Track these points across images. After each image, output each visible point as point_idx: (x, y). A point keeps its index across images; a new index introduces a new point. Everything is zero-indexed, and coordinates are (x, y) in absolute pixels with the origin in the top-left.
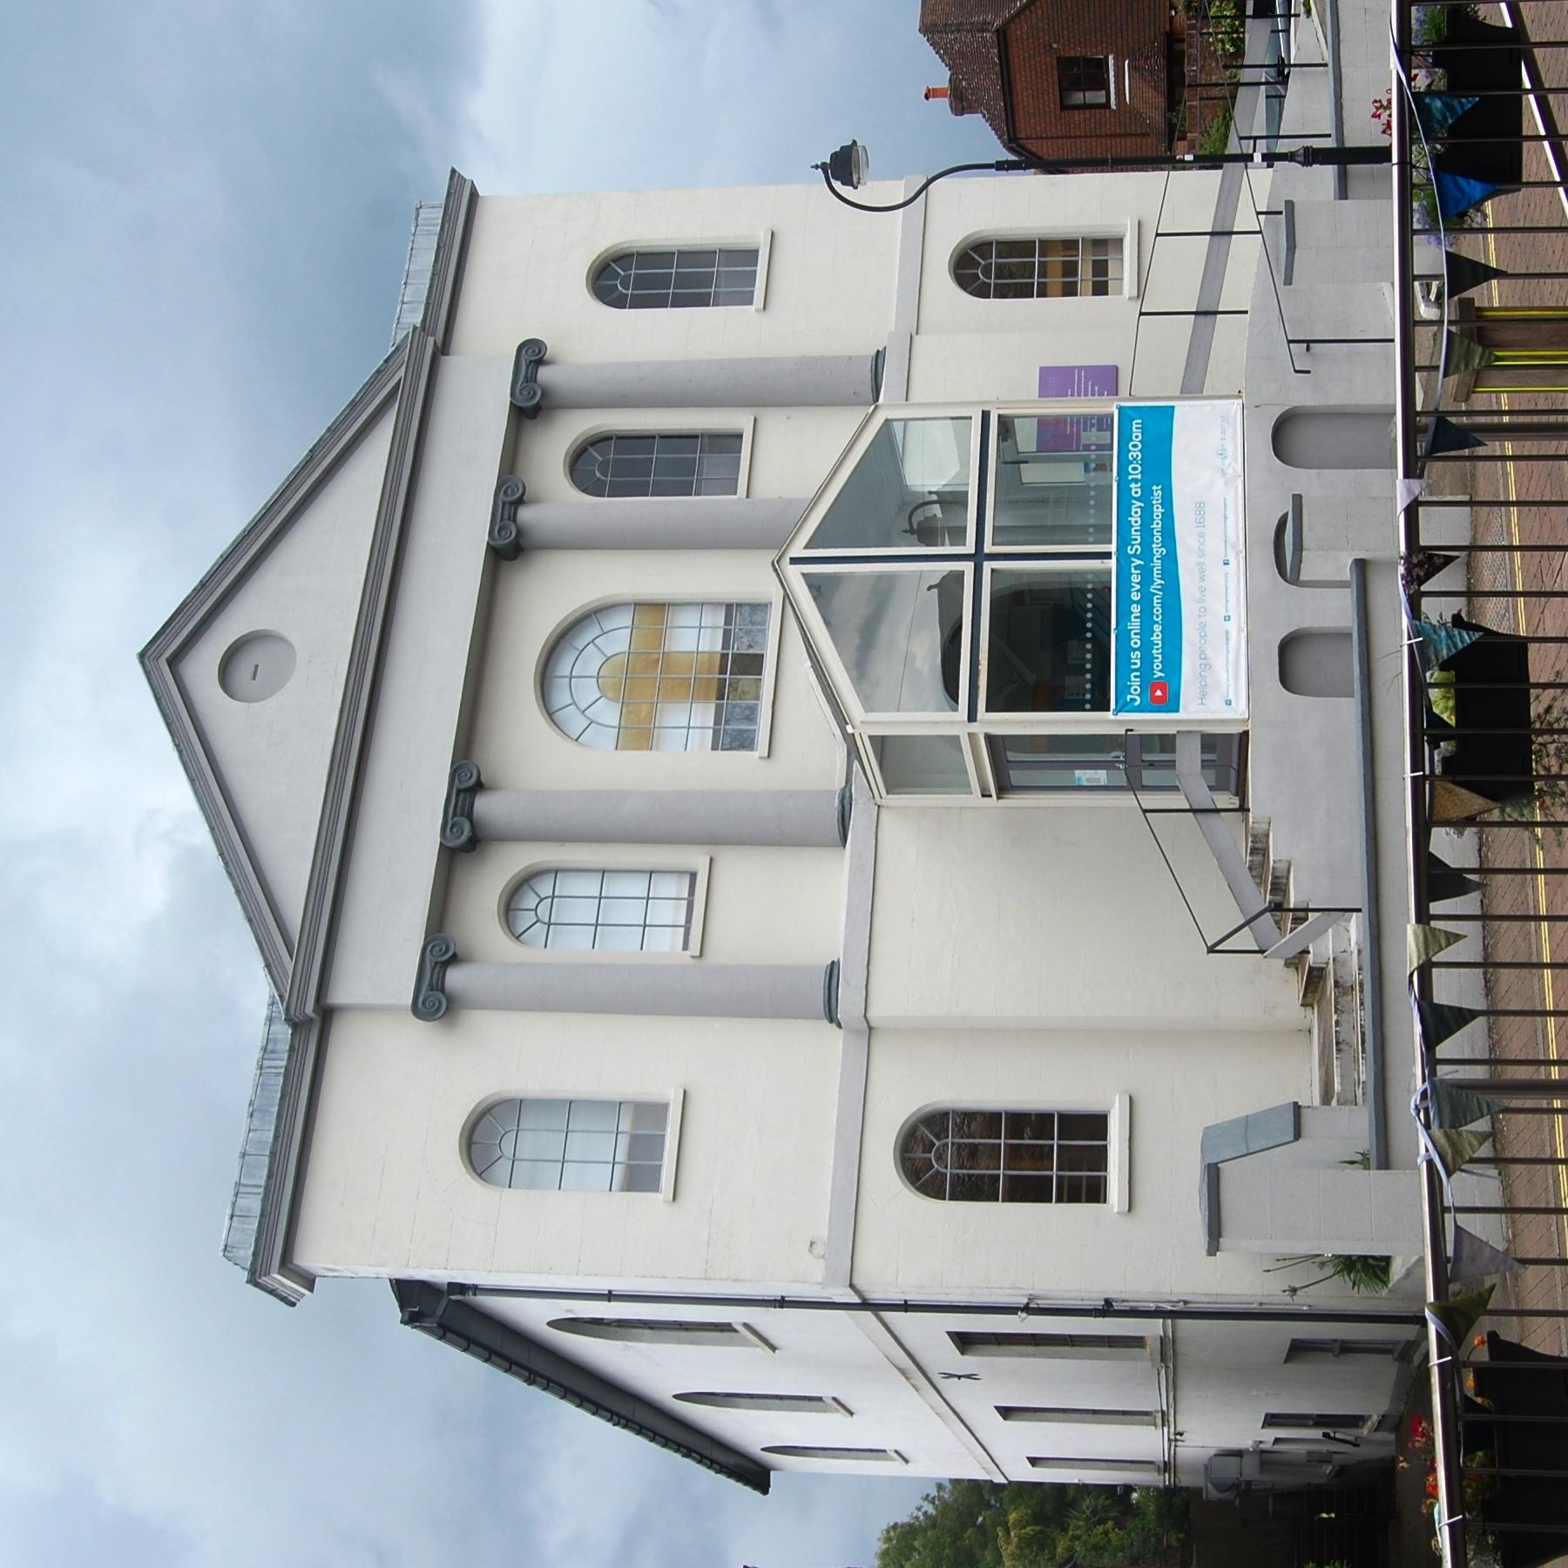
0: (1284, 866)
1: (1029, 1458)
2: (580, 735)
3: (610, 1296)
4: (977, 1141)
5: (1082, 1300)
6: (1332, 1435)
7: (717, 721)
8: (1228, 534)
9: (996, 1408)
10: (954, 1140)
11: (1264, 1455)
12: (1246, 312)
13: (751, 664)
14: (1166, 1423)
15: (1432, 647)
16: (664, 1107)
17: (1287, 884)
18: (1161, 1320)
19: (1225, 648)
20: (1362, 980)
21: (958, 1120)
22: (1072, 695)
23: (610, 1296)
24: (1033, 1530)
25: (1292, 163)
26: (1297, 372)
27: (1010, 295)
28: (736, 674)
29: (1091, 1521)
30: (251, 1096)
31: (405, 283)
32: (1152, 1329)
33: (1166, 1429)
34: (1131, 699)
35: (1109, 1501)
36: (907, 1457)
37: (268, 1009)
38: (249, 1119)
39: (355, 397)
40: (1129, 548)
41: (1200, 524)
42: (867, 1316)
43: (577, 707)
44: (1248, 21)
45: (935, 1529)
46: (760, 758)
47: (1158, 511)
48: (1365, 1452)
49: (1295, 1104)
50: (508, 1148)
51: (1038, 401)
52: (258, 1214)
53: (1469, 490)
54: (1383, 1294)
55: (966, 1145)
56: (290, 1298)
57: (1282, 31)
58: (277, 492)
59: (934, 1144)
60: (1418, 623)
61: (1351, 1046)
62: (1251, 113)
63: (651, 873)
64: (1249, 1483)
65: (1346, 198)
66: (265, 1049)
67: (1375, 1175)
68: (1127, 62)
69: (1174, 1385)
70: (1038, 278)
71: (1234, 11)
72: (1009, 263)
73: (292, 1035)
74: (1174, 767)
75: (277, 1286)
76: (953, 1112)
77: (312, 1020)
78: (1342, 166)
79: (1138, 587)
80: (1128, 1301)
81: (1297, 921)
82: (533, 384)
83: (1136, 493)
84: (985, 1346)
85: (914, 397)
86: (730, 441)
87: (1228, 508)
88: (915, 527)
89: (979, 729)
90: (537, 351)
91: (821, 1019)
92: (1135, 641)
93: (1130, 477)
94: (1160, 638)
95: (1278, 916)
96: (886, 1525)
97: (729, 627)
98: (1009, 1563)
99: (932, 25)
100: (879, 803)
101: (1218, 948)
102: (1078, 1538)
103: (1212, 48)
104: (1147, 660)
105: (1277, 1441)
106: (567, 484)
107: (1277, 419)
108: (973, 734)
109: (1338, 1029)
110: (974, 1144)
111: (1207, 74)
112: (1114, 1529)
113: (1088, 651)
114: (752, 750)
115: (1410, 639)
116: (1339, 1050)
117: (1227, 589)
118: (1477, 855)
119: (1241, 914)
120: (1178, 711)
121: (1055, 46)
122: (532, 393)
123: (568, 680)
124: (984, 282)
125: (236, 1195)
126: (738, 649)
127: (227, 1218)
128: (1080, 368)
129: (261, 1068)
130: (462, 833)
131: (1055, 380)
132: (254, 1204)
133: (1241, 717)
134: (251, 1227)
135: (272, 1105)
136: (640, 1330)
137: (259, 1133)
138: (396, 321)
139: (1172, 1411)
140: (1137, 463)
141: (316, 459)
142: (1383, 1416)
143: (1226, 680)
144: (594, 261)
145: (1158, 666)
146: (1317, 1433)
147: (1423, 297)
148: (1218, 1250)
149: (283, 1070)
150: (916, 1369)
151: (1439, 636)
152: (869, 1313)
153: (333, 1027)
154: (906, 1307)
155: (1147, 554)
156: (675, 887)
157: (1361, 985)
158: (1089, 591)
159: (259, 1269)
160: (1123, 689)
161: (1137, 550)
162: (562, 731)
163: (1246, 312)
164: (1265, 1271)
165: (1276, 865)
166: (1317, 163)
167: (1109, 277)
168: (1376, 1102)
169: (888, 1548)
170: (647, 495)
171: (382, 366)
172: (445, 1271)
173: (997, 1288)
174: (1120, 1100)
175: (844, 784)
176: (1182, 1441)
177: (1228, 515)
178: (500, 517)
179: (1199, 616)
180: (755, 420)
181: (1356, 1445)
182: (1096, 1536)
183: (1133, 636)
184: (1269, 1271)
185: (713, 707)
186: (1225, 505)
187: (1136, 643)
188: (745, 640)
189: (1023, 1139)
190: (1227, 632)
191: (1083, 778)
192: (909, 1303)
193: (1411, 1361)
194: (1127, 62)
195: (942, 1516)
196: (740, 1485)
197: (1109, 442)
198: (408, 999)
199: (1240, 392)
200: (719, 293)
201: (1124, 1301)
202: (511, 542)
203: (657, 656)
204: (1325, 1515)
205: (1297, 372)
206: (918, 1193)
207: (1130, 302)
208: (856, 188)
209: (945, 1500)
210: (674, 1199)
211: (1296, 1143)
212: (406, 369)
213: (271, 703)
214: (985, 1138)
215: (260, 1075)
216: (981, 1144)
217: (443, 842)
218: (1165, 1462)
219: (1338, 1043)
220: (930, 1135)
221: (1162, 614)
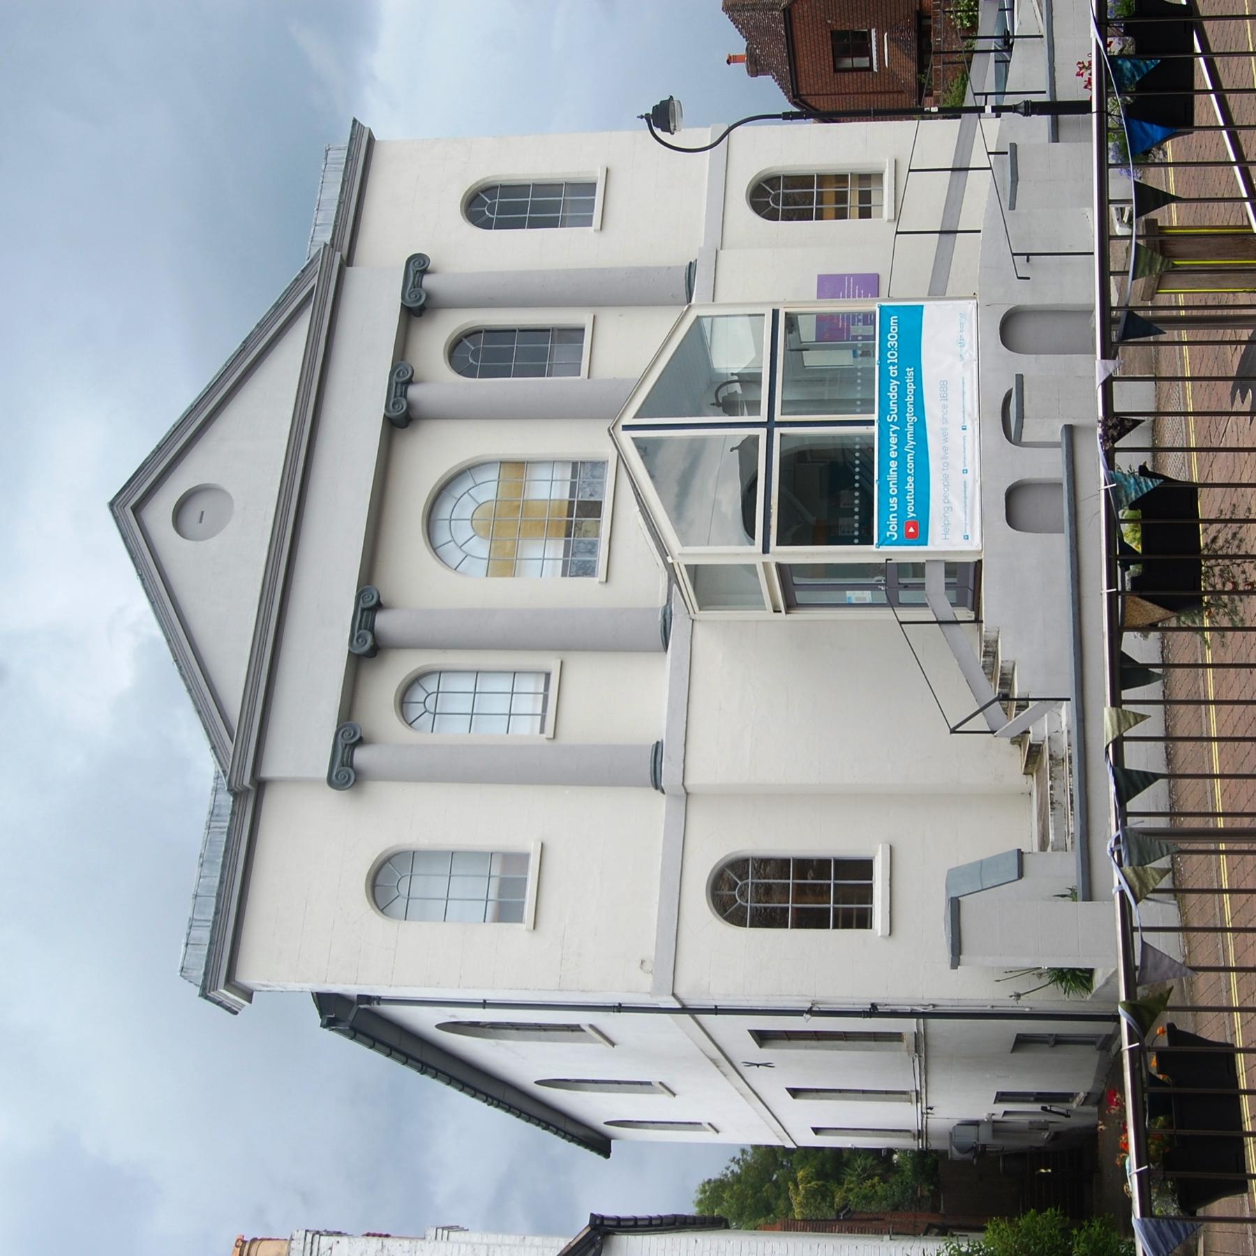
3: (485, 1004)
4: (771, 881)
6: (1049, 1108)
7: (566, 554)
9: (787, 1089)
11: (995, 1124)
12: (979, 231)
13: (593, 509)
15: (1123, 492)
17: (1012, 679)
22: (844, 532)
23: (485, 1004)
24: (816, 1184)
26: (1019, 278)
31: (318, 209)
32: (908, 1026)
33: (919, 1105)
34: (890, 535)
35: (875, 1161)
39: (279, 300)
42: (686, 1018)
46: (600, 582)
47: (911, 387)
48: (1074, 1122)
49: (1019, 850)
50: (403, 888)
51: (816, 302)
52: (208, 942)
55: (761, 883)
57: (1007, 9)
58: (218, 374)
61: (1062, 806)
62: (983, 74)
64: (984, 1146)
65: (1058, 142)
66: (212, 813)
67: (1081, 904)
68: (886, 35)
69: (925, 1070)
72: (793, 193)
74: (923, 588)
76: (752, 858)
77: (248, 790)
79: (896, 447)
81: (1020, 708)
83: (894, 373)
84: (778, 1041)
85: (719, 299)
88: (721, 401)
89: (772, 559)
90: (422, 263)
91: (649, 786)
92: (893, 490)
93: (889, 361)
101: (958, 730)
102: (851, 1190)
104: (902, 503)
105: (1006, 1113)
110: (769, 884)
112: (879, 1183)
113: (856, 498)
114: (594, 576)
115: (1106, 485)
116: (1053, 809)
117: (965, 448)
120: (926, 545)
121: (829, 22)
123: (448, 522)
124: (774, 208)
125: (190, 927)
127: (183, 946)
128: (850, 276)
130: (366, 642)
131: (830, 285)
132: (204, 935)
136: (508, 1031)
137: (207, 879)
139: (924, 1090)
142: (1088, 1093)
146: (1037, 1107)
147: (1118, 219)
149: (226, 830)
150: (725, 1059)
151: (1129, 483)
152: (687, 1015)
154: (716, 1011)
155: (902, 421)
156: (532, 685)
157: (1070, 757)
160: (884, 527)
161: (894, 418)
163: (979, 231)
165: (1003, 665)
172: (354, 986)
177: (967, 495)
181: (1067, 1116)
182: (866, 1188)
183: (891, 486)
185: (562, 542)
187: (893, 491)
188: (588, 490)
189: (807, 879)
190: (965, 482)
193: (1109, 1050)
194: (886, 35)
197: (872, 333)
201: (886, 1005)
203: (518, 503)
204: (1043, 1171)
205: (1019, 278)
209: (747, 1161)
210: (534, 928)
211: (1020, 881)
213: (213, 543)
214: (777, 879)
216: (774, 883)
217: (351, 650)
218: (919, 1131)
219: (1052, 803)
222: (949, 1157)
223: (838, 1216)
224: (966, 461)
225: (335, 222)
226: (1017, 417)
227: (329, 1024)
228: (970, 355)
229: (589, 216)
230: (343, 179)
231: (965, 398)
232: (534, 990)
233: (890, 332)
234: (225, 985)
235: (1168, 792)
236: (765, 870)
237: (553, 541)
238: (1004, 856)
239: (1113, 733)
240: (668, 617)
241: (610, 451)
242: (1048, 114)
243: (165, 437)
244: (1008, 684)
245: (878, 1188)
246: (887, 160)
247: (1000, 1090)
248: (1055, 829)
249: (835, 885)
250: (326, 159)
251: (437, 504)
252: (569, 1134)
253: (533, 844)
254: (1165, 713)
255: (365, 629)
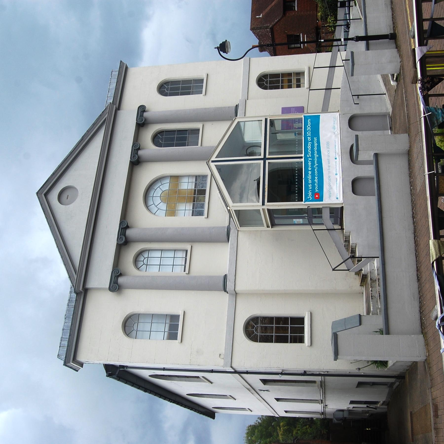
0: (355, 245)
1: (285, 411)
2: (156, 212)
3: (164, 369)
4: (267, 325)
5: (298, 371)
6: (369, 406)
8: (336, 151)
9: (275, 398)
10: (260, 325)
11: (350, 411)
12: (340, 88)
13: (203, 192)
14: (322, 403)
15: (435, 118)
16: (179, 316)
17: (355, 251)
18: (320, 377)
19: (336, 183)
20: (379, 278)
21: (261, 319)
23: (164, 369)
24: (287, 428)
25: (353, 41)
26: (355, 104)
27: (273, 89)
28: (198, 195)
29: (303, 425)
30: (66, 313)
31: (108, 92)
32: (318, 379)
33: (322, 404)
34: (309, 198)
35: (307, 420)
36: (252, 410)
37: (70, 289)
38: (65, 320)
39: (94, 122)
40: (308, 155)
41: (328, 148)
42: (237, 375)
43: (155, 205)
44: (338, 9)
45: (261, 426)
46: (205, 218)
47: (316, 144)
48: (378, 410)
49: (360, 315)
50: (135, 328)
51: (281, 115)
52: (67, 346)
53: (408, 132)
54: (386, 370)
55: (263, 326)
56: (76, 369)
57: (347, 14)
58: (73, 148)
59: (255, 326)
60: (428, 107)
61: (375, 297)
62: (340, 34)
63: (175, 250)
64: (345, 418)
65: (369, 50)
66: (69, 300)
67: (385, 336)
68: (305, 35)
69: (324, 393)
70: (281, 84)
71: (334, 19)
72: (273, 80)
73: (76, 296)
74: (322, 218)
75: (72, 366)
76: (260, 317)
77: (82, 292)
78: (367, 41)
79: (311, 166)
80: (311, 371)
81: (359, 261)
82: (143, 117)
83: (309, 140)
84: (271, 383)
85: (247, 115)
86: (196, 131)
87: (336, 143)
88: (248, 154)
89: (265, 207)
90: (143, 108)
91: (222, 291)
92: (310, 182)
93: (308, 135)
94: (317, 180)
95: (353, 260)
96: (248, 425)
97: (196, 182)
98: (281, 436)
99: (253, 28)
100: (238, 230)
101: (335, 269)
102: (299, 430)
103: (328, 29)
104: (313, 187)
105: (353, 407)
106: (152, 145)
107: (350, 117)
108: (264, 209)
109: (371, 292)
110: (266, 326)
111: (327, 36)
112: (309, 427)
114: (203, 216)
115: (424, 114)
117: (336, 166)
118: (414, 240)
119: (342, 259)
120: (323, 201)
121: (286, 32)
122: (142, 120)
123: (152, 197)
124: (266, 85)
125: (61, 341)
126: (199, 188)
127: (59, 347)
128: (293, 107)
129: (68, 305)
130: (123, 240)
131: (285, 110)
132: (66, 343)
133: (341, 202)
134: (65, 350)
135: (71, 316)
136: (175, 378)
138: (106, 102)
139: (324, 400)
140: (310, 131)
141: (84, 139)
142: (384, 402)
143: (336, 192)
144: (159, 84)
145: (317, 189)
146: (365, 406)
147: (392, 79)
148: (337, 359)
149: (74, 306)
150: (252, 388)
151: (438, 112)
152: (237, 374)
153: (88, 292)
154: (247, 373)
155: (313, 157)
156: (181, 254)
157: (379, 279)
158: (296, 170)
159: (67, 361)
160: (307, 195)
161: (310, 156)
162: (151, 212)
163: (340, 88)
164: (351, 363)
165: (352, 245)
166: (360, 41)
167: (301, 83)
168: (385, 314)
169: (248, 432)
170: (174, 147)
171: (101, 114)
172: (118, 362)
173: (273, 368)
174: (308, 313)
175: (228, 225)
176: (327, 407)
177: (337, 169)
178: (133, 153)
179: (328, 174)
180: (203, 125)
181: (376, 409)
182: (304, 429)
183: (309, 180)
184: (352, 363)
185: (192, 204)
186: (335, 142)
187: (310, 182)
188: (201, 185)
189: (280, 325)
190: (336, 178)
191: (296, 221)
192: (248, 371)
193: (393, 387)
194: (305, 35)
195: (263, 423)
196: (207, 417)
197: (302, 126)
198: (108, 286)
199: (339, 110)
200: (193, 91)
201: (310, 371)
202: (136, 160)
203: (176, 190)
204: (367, 429)
205: (355, 104)
206: (250, 340)
207: (307, 89)
208: (227, 54)
209: (264, 419)
210: (181, 342)
211: (360, 326)
212: (108, 114)
213: (71, 206)
214: (269, 325)
215: (68, 307)
216: (268, 326)
217: (117, 242)
218: (322, 412)
219: (372, 297)
220: (253, 324)
221: (317, 174)
222: (333, 422)
223: (294, 442)
224: (337, 170)
225: (114, 95)
226: (356, 151)
227: (109, 375)
228: (337, 132)
229: (201, 90)
230: (117, 81)
231: (336, 148)
232: (181, 364)
233: (308, 125)
234: (72, 361)
235: (418, 292)
236: (265, 321)
237: (189, 204)
238: (354, 317)
239: (436, 255)
240: (229, 230)
241: (209, 171)
242: (365, 41)
243: (55, 170)
244: (354, 252)
245: (308, 430)
246: (306, 67)
247: (351, 400)
248: (373, 306)
249: (290, 326)
250: (111, 74)
251: (148, 191)
252: (200, 411)
253: (181, 312)
254: (416, 262)
255: (122, 235)
